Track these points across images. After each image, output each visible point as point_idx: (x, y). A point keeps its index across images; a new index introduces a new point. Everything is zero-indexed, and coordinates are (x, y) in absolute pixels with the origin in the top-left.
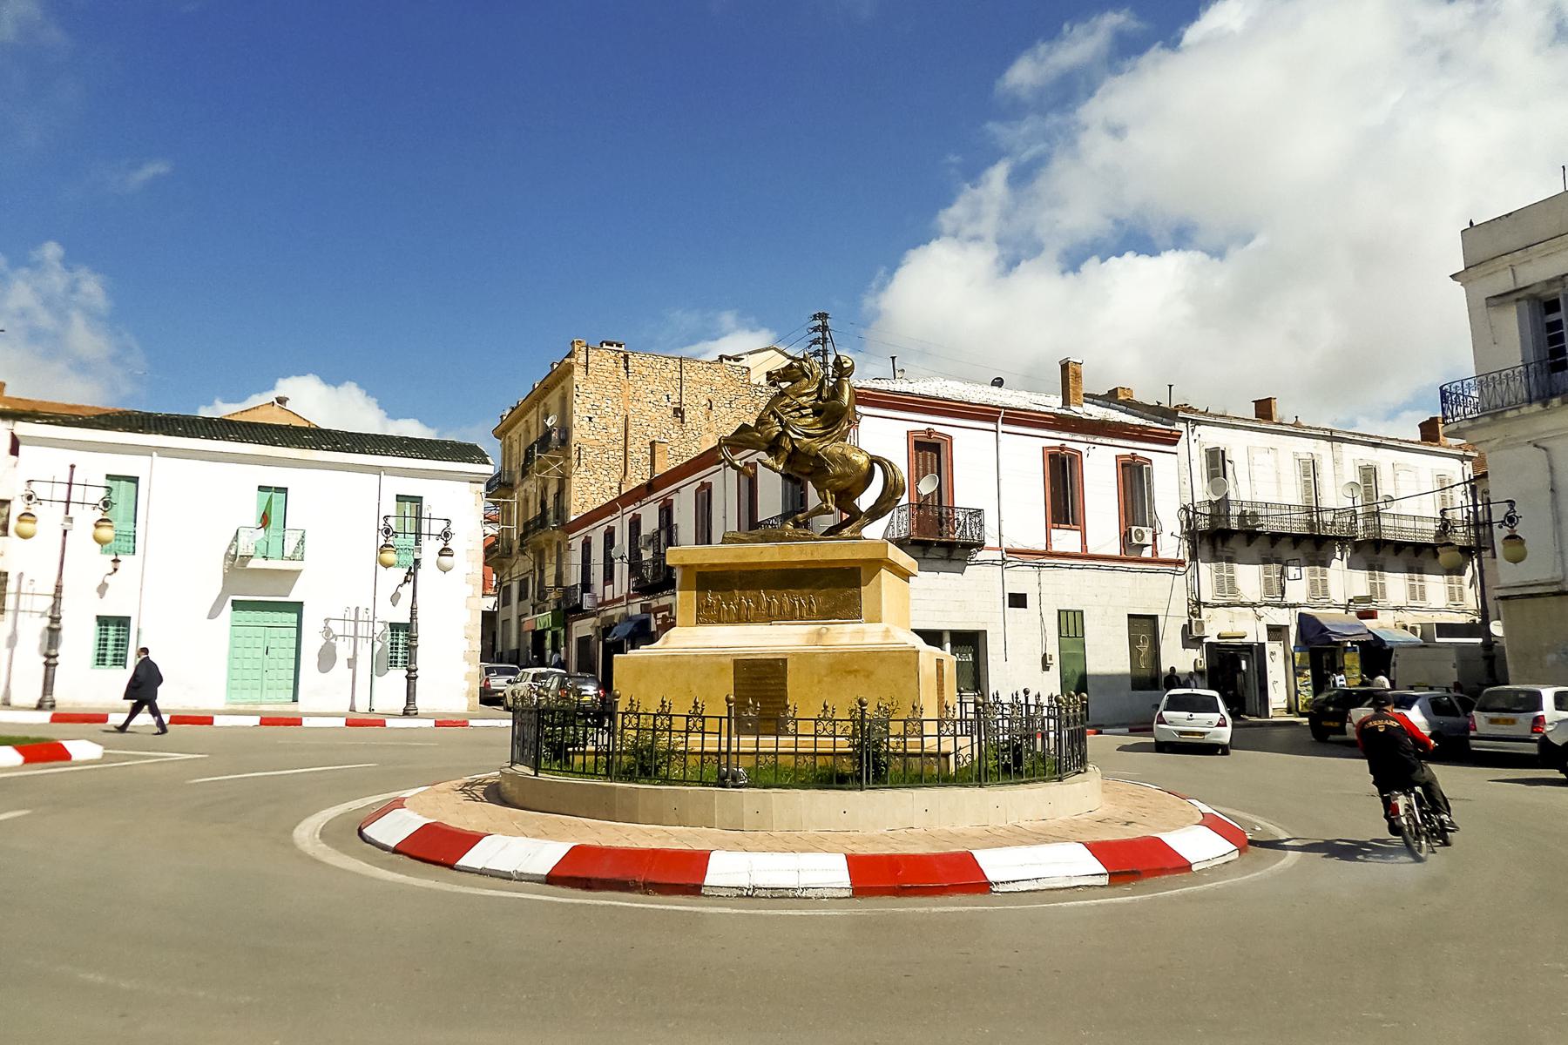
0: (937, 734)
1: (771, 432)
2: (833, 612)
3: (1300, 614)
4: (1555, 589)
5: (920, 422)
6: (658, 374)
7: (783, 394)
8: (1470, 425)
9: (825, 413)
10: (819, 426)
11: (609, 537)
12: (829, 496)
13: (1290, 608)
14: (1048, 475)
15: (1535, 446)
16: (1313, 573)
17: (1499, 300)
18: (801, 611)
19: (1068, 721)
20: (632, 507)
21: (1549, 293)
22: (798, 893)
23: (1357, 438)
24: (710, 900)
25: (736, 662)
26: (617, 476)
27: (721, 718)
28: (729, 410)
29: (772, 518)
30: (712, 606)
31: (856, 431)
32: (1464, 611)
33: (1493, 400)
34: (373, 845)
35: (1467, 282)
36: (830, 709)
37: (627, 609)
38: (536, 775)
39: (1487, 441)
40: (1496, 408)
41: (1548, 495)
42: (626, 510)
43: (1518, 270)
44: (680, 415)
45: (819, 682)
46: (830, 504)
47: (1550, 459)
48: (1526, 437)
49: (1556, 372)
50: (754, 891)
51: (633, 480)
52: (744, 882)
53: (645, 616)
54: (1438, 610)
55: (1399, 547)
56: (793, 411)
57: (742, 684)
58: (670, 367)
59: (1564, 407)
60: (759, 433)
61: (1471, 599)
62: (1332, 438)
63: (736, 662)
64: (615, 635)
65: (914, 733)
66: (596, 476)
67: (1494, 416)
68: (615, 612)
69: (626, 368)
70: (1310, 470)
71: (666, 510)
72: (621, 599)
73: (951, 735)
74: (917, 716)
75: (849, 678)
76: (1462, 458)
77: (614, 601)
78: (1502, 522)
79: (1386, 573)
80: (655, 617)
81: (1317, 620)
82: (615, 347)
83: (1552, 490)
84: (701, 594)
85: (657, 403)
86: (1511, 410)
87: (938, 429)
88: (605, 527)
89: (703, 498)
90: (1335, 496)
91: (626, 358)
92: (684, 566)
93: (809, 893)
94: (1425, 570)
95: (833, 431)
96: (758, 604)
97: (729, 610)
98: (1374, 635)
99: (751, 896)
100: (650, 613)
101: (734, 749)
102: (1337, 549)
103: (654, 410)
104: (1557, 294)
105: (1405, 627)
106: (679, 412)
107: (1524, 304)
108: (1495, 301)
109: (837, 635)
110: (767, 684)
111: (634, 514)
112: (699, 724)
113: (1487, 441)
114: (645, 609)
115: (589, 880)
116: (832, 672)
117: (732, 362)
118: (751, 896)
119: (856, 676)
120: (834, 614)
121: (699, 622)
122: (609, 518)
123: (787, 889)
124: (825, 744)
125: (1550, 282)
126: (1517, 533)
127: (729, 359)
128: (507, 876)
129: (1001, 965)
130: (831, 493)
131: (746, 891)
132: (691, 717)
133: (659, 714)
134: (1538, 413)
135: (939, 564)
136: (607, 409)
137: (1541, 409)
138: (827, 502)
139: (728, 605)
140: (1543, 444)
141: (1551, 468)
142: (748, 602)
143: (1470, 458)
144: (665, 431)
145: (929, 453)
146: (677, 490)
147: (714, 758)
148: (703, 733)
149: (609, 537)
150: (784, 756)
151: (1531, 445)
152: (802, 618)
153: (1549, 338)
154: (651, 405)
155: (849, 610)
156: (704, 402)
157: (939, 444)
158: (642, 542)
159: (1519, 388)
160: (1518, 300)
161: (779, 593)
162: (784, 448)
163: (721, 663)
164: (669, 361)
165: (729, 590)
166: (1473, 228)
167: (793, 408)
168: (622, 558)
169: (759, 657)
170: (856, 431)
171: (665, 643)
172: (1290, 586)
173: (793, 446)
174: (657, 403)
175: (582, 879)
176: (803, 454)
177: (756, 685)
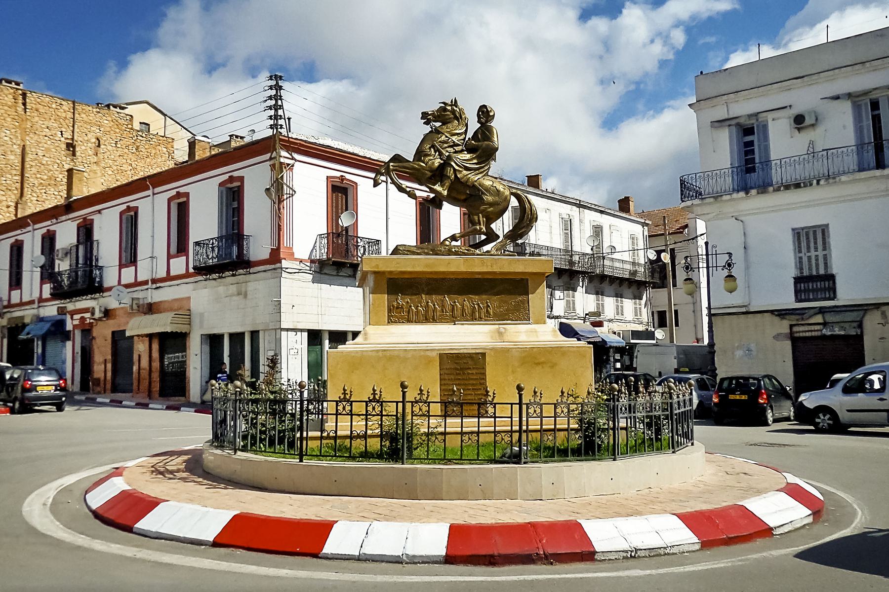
0: (335, 413)
1: (433, 163)
3: (560, 323)
4: (744, 310)
5: (336, 170)
6: (53, 113)
7: (437, 131)
8: (700, 202)
9: (480, 151)
10: (475, 161)
12: (481, 219)
13: (555, 319)
14: (418, 218)
15: (736, 219)
16: (568, 296)
17: (720, 123)
18: (480, 313)
19: (685, 403)
20: (49, 223)
21: (749, 122)
22: (668, 551)
23: (593, 207)
24: (601, 565)
25: (441, 356)
26: (13, 197)
27: (397, 402)
28: (114, 148)
29: (212, 239)
30: (402, 307)
31: (291, 173)
32: (641, 323)
33: (715, 188)
34: (171, 540)
35: (698, 110)
36: (425, 392)
37: (38, 311)
38: (301, 461)
39: (708, 214)
40: (709, 194)
41: (743, 250)
43: (730, 106)
44: (71, 149)
45: (513, 372)
46: (482, 227)
47: (744, 225)
50: (636, 553)
51: (28, 201)
52: (626, 547)
53: (60, 317)
54: (630, 322)
55: (613, 280)
56: (449, 147)
57: (448, 374)
58: (64, 107)
60: (424, 163)
61: (645, 316)
62: (580, 205)
63: (441, 356)
64: (28, 334)
65: (535, 414)
67: (716, 198)
68: (28, 314)
69: (24, 104)
70: (568, 225)
71: (86, 231)
72: (32, 302)
73: (348, 414)
74: (537, 400)
76: (644, 225)
77: (22, 304)
78: (724, 266)
79: (624, 299)
80: (72, 318)
81: (572, 327)
82: (13, 85)
83: (745, 248)
84: (393, 297)
85: (51, 137)
87: (348, 176)
90: (582, 245)
91: (24, 95)
92: (375, 273)
93: (674, 550)
94: (624, 296)
95: (483, 167)
97: (418, 312)
98: (602, 339)
99: (634, 557)
100: (65, 314)
101: (524, 428)
102: (581, 280)
103: (49, 142)
104: (753, 124)
105: (615, 333)
106: (71, 147)
107: (734, 129)
108: (716, 124)
109: (515, 334)
110: (469, 374)
111: (48, 230)
112: (348, 408)
113: (708, 214)
114: (62, 311)
115: (492, 556)
117: (118, 110)
118: (634, 557)
119: (543, 367)
120: (507, 317)
121: (390, 322)
122: (19, 232)
123: (660, 548)
124: (562, 423)
125: (750, 116)
127: (115, 107)
128: (397, 560)
130: (483, 217)
131: (630, 553)
132: (340, 402)
133: (370, 401)
134: (742, 198)
135: (347, 280)
136: (6, 138)
137: (744, 196)
138: (480, 224)
139: (417, 307)
141: (744, 233)
142: (434, 305)
143: (647, 225)
144: (58, 161)
145: (340, 195)
146: (99, 212)
147: (440, 437)
148: (542, 417)
151: (734, 218)
152: (480, 318)
153: (745, 151)
154: (46, 138)
155: (521, 314)
156: (94, 140)
157: (347, 188)
159: (728, 182)
160: (729, 125)
161: (461, 298)
162: (449, 177)
163: (428, 356)
164: (63, 103)
165: (416, 294)
166: (702, 76)
167: (448, 144)
169: (461, 351)
170: (291, 173)
172: (556, 303)
173: (456, 176)
174: (51, 137)
175: (485, 556)
176: (462, 182)
177: (459, 374)
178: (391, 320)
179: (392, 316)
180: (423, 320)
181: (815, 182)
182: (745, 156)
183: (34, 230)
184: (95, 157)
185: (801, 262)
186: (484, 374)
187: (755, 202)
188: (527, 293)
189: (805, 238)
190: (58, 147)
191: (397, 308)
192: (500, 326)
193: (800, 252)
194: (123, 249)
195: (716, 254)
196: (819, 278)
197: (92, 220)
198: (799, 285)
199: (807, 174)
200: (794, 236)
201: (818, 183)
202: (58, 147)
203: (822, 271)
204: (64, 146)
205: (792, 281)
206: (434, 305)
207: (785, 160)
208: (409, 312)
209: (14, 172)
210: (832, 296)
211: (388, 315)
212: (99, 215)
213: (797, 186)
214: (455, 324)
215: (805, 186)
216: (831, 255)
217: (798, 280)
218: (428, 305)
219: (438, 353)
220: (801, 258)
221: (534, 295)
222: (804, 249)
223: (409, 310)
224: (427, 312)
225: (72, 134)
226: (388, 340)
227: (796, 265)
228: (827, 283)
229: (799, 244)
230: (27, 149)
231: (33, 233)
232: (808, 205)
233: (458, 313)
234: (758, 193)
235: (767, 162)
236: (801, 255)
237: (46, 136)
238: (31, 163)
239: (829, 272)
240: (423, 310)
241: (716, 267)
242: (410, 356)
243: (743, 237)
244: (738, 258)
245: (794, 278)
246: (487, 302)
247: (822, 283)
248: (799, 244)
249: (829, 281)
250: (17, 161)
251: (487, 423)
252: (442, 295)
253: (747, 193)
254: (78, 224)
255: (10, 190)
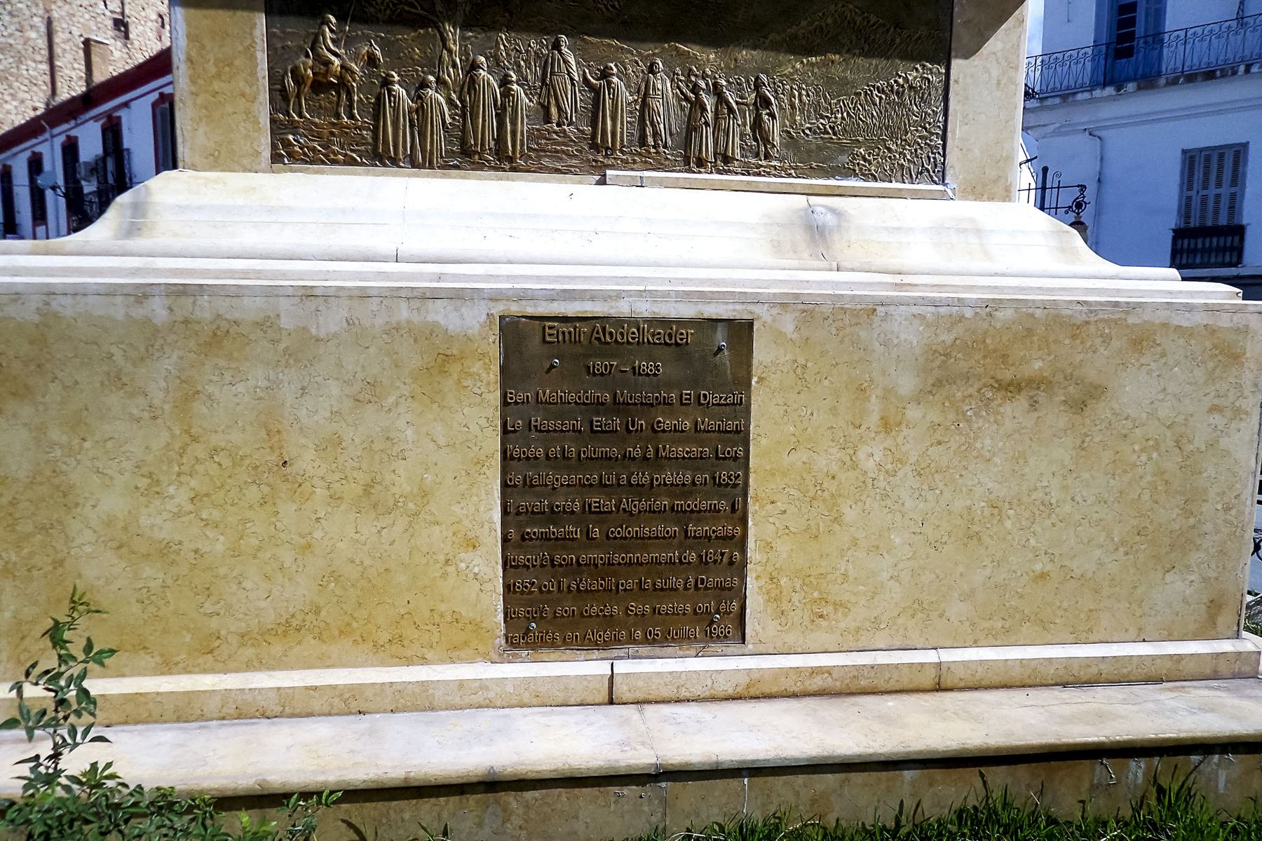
2: (842, 149)
8: (1038, 105)
11: (35, 165)
15: (1090, 134)
20: (65, 127)
26: (42, 95)
39: (1044, 126)
42: (56, 130)
44: (123, 29)
45: (887, 426)
47: (1102, 147)
48: (1084, 123)
49: (1121, 59)
59: (1139, 93)
66: (12, 91)
67: (1064, 98)
71: (112, 131)
75: (1007, 409)
78: (1070, 207)
83: (1099, 180)
84: (296, 27)
85: (90, 8)
86: (1082, 92)
88: (28, 154)
89: (163, 115)
96: (546, 87)
113: (1044, 126)
116: (939, 384)
119: (1034, 405)
122: (34, 141)
126: (1082, 220)
129: (396, 543)
140: (1097, 133)
141: (1102, 158)
142: (505, 82)
146: (126, 105)
149: (35, 165)
150: (801, 779)
151: (1087, 132)
152: (725, 160)
156: (154, 17)
158: (82, 171)
163: (432, 331)
165: (413, 22)
168: (54, 188)
171: (132, 230)
178: (286, 144)
179: (293, 127)
180: (450, 154)
181: (1242, 68)
182: (1118, 30)
183: (53, 136)
184: (158, 43)
185: (1188, 206)
186: (741, 434)
187: (1138, 104)
188: (941, 52)
189: (1202, 166)
190: (100, 23)
191: (319, 86)
192: (813, 199)
193: (1190, 188)
194: (161, 161)
195: (1059, 188)
196: (1216, 231)
197: (119, 118)
198: (1180, 242)
199: (1230, 55)
200: (1184, 162)
201: (1247, 70)
202: (100, 23)
203: (1223, 221)
204: (110, 23)
205: (1171, 234)
206: (505, 82)
207: (1193, 30)
208: (377, 111)
209: (38, 58)
210: (1235, 259)
211: (273, 121)
212: (126, 110)
213: (1210, 75)
214: (602, 182)
215: (1223, 76)
216: (1243, 195)
217: (1179, 234)
218: (473, 81)
219: (498, 309)
220: (1189, 198)
221: (975, 60)
222: (1196, 185)
223: (379, 98)
224: (466, 112)
225: (120, 5)
226: (250, 238)
227: (1179, 211)
228: (1186, 242)
229: (1191, 175)
230: (55, 24)
231: (52, 141)
232: (1218, 110)
233: (622, 127)
234: (1139, 88)
235: (1156, 37)
236: (1190, 193)
237: (81, 6)
238: (62, 45)
239: (1236, 222)
240: (450, 102)
241: (1056, 208)
242: (333, 328)
243: (1098, 163)
244: (1090, 195)
245: (1174, 231)
246: (758, 85)
247: (1193, 242)
248: (1191, 175)
249: (1189, 239)
250: (42, 43)
251: (743, 680)
252: (544, 31)
253: (1118, 89)
254: (102, 126)
255: (35, 85)
